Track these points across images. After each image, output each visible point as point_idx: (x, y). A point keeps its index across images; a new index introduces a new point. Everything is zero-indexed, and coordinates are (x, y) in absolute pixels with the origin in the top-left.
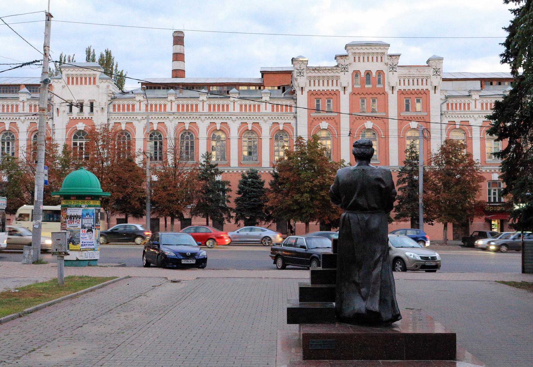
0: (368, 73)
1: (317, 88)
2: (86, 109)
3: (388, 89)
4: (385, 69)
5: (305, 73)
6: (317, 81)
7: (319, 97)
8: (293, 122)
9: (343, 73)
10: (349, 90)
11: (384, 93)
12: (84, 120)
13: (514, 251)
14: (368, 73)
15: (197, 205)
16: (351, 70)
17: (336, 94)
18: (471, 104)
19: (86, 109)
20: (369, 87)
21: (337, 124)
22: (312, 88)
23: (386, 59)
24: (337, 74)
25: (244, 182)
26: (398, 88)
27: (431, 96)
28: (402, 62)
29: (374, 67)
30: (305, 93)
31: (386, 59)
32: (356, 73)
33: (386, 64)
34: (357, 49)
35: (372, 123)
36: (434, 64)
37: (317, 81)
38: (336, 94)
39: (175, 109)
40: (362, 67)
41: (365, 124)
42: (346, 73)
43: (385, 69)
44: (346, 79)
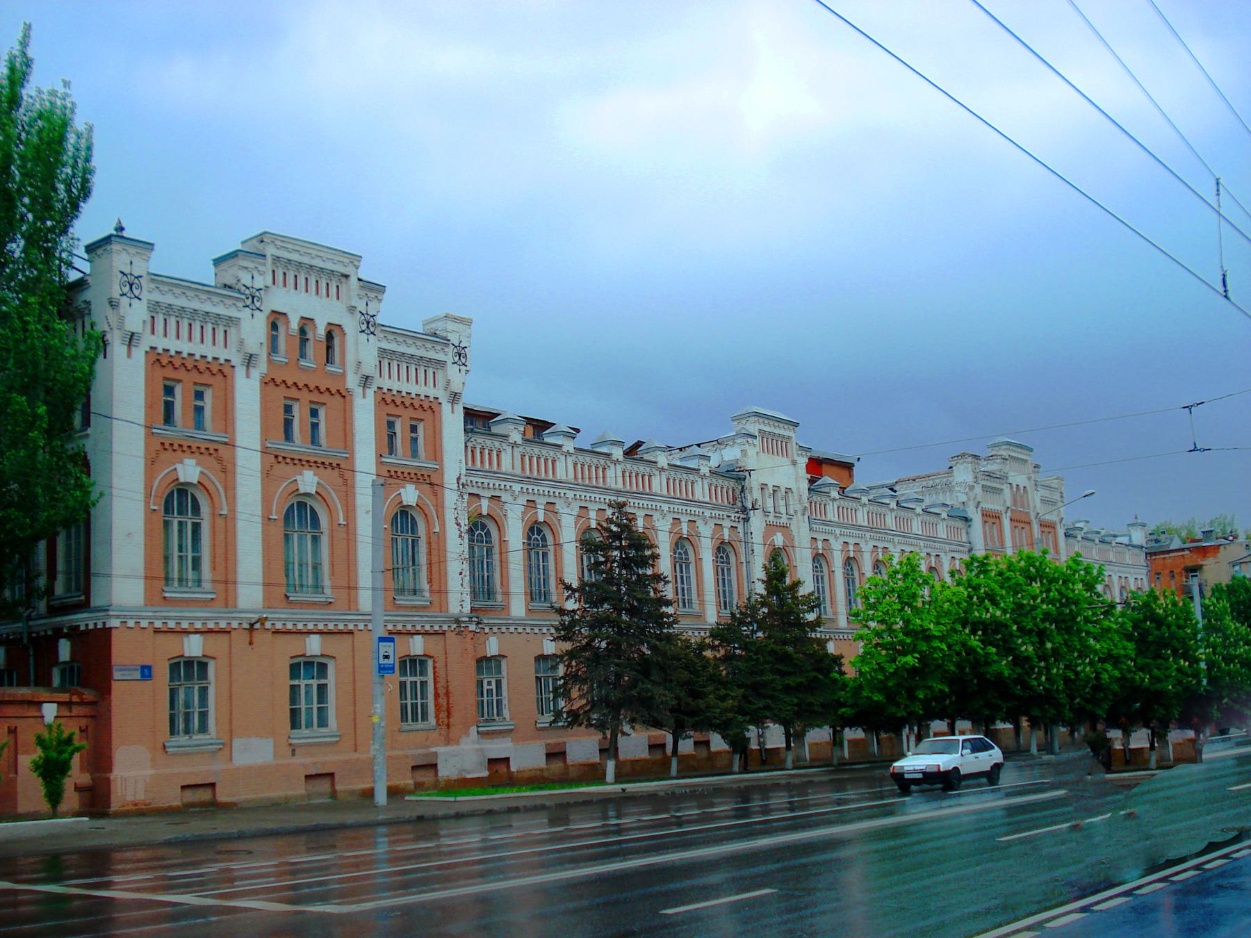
0: (306, 323)
1: (173, 345)
3: (352, 382)
4: (351, 325)
5: (145, 292)
6: (208, 329)
7: (321, 399)
9: (248, 311)
10: (261, 368)
11: (344, 395)
13: (558, 868)
14: (306, 323)
15: (372, 770)
18: (557, 463)
21: (224, 471)
22: (161, 343)
24: (233, 313)
26: (147, 341)
27: (444, 417)
29: (324, 311)
30: (139, 354)
32: (276, 320)
33: (352, 309)
35: (199, 469)
37: (208, 329)
38: (221, 372)
40: (296, 303)
41: (179, 466)
42: (257, 313)
44: (253, 330)
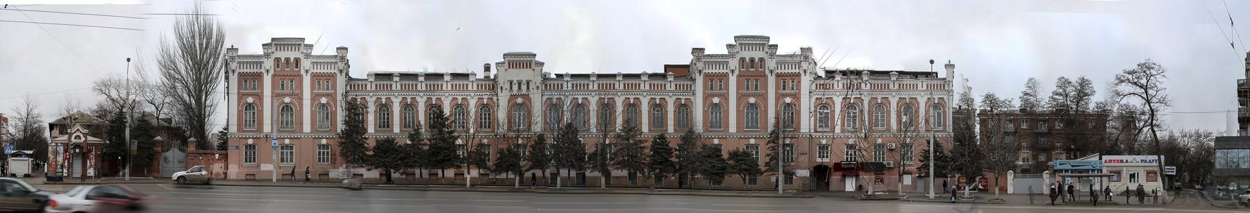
0: (752, 60)
2: (524, 87)
4: (302, 57)
8: (945, 98)
10: (737, 72)
11: (765, 76)
12: (522, 96)
14: (752, 60)
16: (273, 57)
17: (726, 75)
19: (524, 87)
20: (752, 72)
23: (766, 49)
25: (655, 142)
26: (238, 71)
28: (315, 52)
29: (757, 55)
31: (766, 49)
32: (743, 60)
34: (743, 41)
36: (806, 53)
38: (726, 75)
39: (647, 88)
40: (747, 55)
43: (302, 57)
